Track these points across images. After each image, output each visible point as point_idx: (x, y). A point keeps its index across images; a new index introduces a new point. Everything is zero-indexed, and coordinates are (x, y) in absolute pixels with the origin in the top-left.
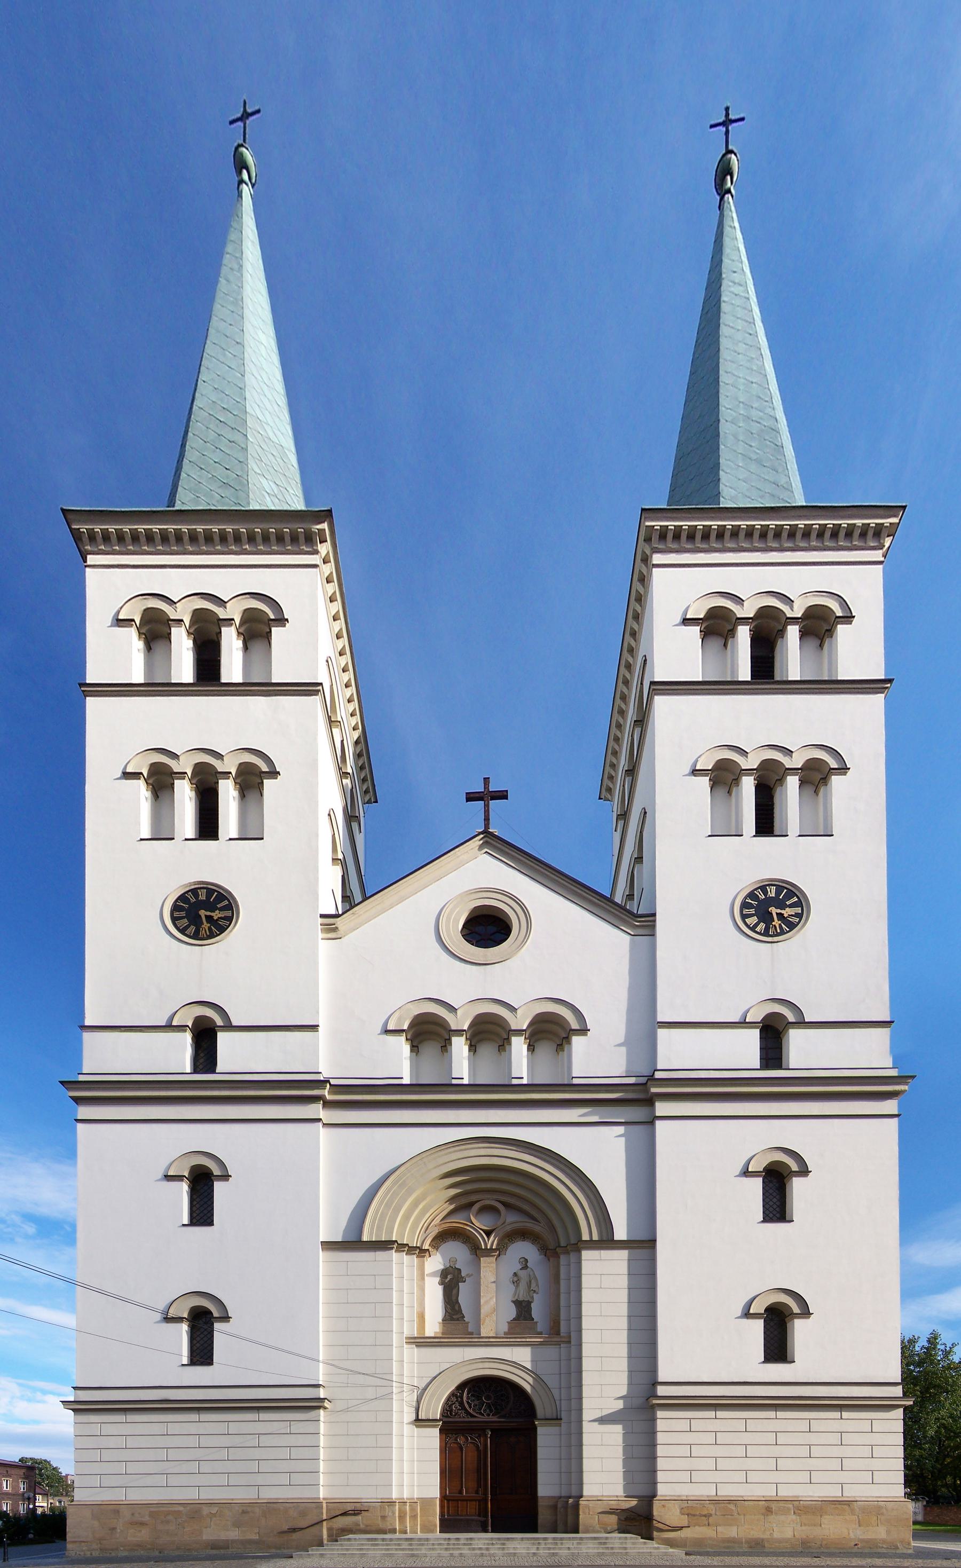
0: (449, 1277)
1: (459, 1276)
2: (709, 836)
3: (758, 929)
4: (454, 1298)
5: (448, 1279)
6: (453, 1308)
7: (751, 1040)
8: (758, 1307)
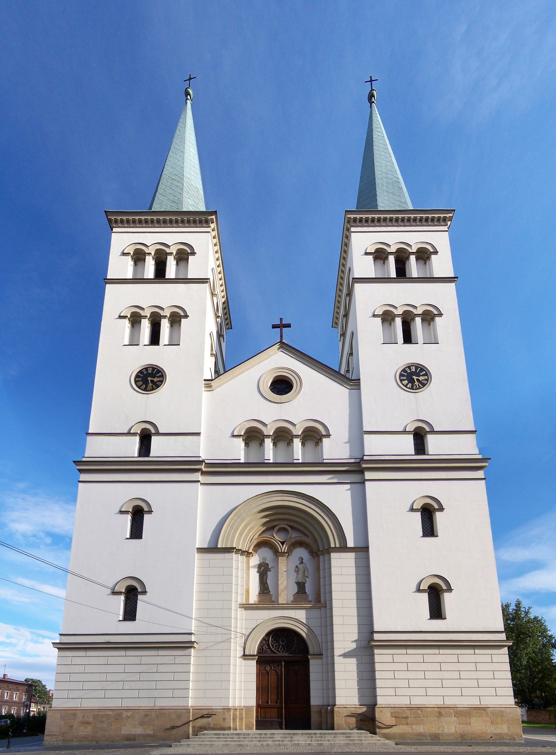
0: (262, 568)
1: (268, 568)
2: (383, 344)
3: (408, 386)
4: (265, 581)
5: (262, 570)
6: (264, 587)
7: (410, 438)
8: (424, 586)
